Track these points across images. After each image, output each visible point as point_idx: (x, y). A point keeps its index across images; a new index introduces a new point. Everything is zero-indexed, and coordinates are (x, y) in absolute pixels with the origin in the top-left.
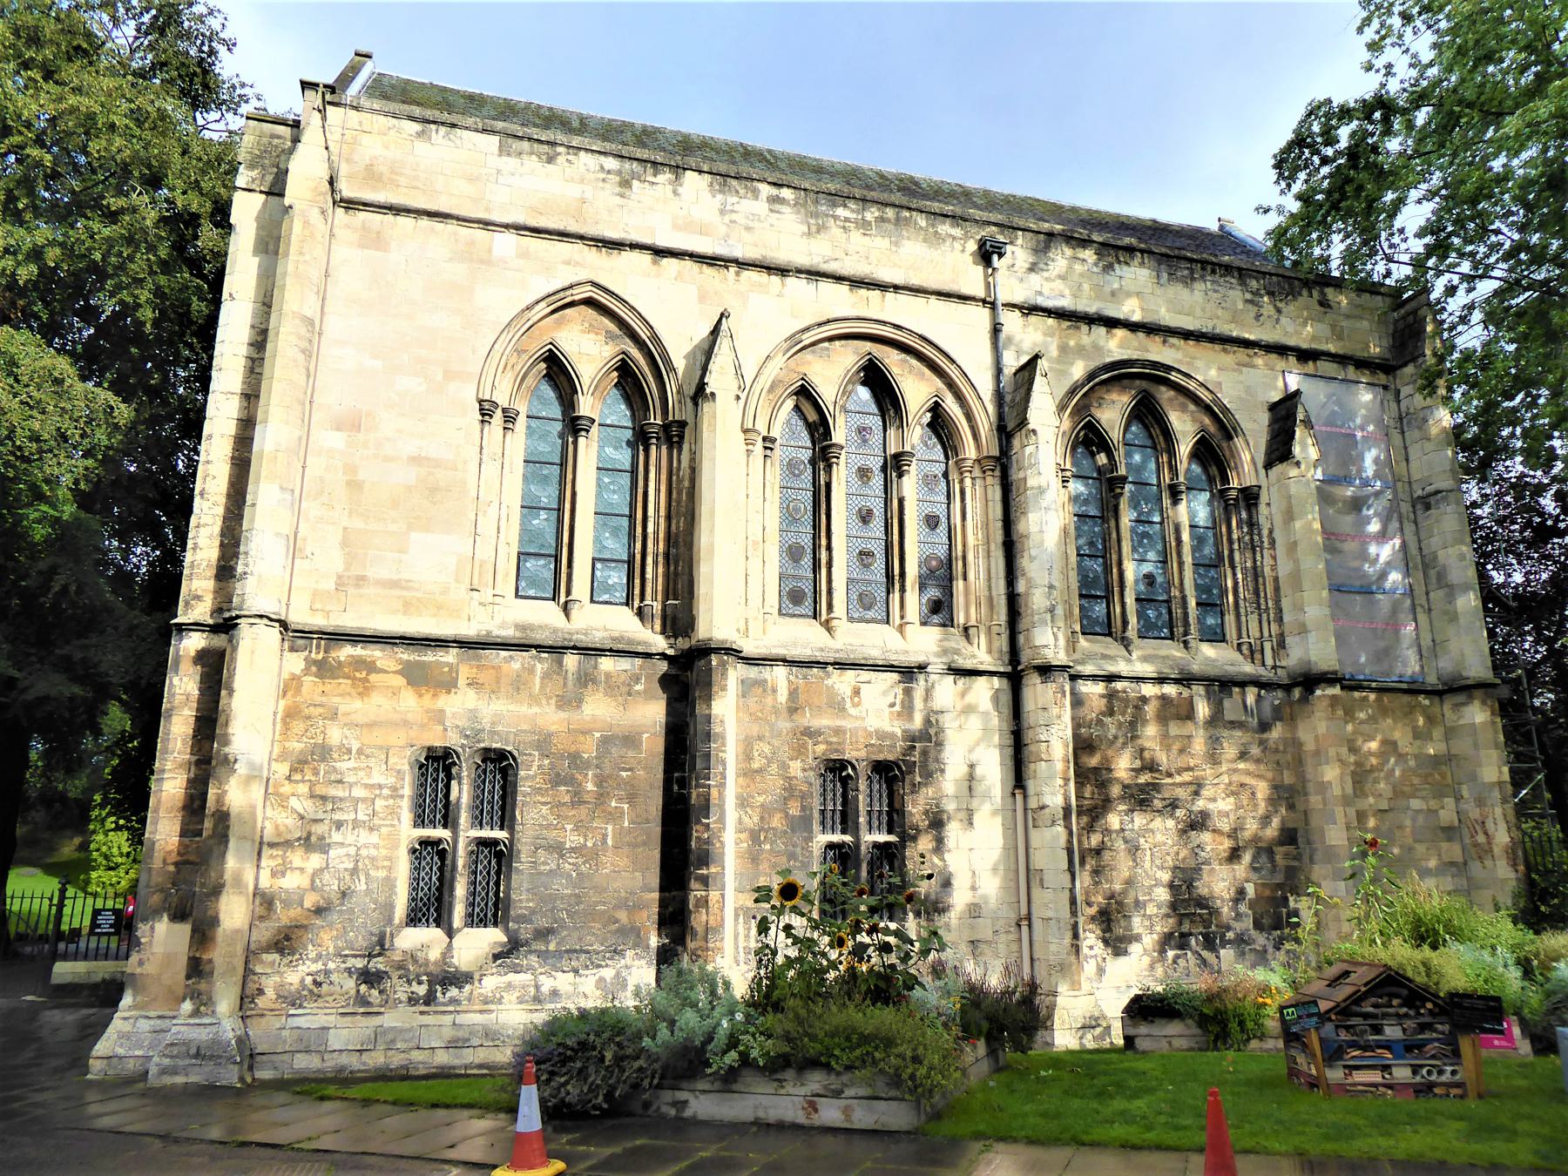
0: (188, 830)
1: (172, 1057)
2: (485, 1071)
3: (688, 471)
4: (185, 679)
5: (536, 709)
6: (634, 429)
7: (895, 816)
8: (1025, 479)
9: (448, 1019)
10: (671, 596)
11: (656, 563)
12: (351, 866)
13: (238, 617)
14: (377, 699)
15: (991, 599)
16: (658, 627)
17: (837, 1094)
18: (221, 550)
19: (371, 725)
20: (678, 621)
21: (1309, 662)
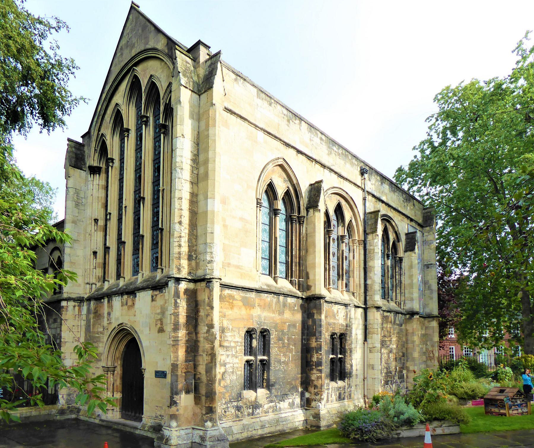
0: (188, 360)
1: (212, 442)
2: (270, 435)
3: (305, 234)
4: (182, 300)
5: (274, 315)
6: (286, 216)
7: (342, 350)
8: (374, 249)
9: (258, 420)
10: (301, 278)
11: (296, 266)
12: (232, 370)
13: (213, 278)
14: (236, 310)
15: (360, 284)
16: (297, 288)
17: (441, 426)
18: (189, 248)
19: (235, 320)
20: (304, 286)
21: (413, 308)
